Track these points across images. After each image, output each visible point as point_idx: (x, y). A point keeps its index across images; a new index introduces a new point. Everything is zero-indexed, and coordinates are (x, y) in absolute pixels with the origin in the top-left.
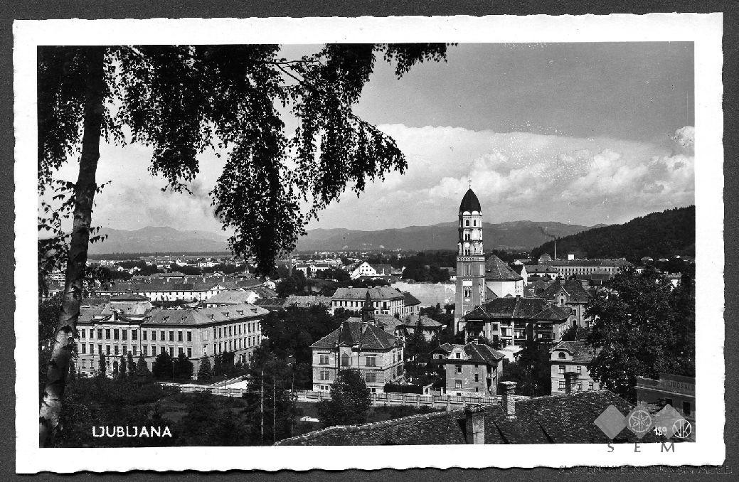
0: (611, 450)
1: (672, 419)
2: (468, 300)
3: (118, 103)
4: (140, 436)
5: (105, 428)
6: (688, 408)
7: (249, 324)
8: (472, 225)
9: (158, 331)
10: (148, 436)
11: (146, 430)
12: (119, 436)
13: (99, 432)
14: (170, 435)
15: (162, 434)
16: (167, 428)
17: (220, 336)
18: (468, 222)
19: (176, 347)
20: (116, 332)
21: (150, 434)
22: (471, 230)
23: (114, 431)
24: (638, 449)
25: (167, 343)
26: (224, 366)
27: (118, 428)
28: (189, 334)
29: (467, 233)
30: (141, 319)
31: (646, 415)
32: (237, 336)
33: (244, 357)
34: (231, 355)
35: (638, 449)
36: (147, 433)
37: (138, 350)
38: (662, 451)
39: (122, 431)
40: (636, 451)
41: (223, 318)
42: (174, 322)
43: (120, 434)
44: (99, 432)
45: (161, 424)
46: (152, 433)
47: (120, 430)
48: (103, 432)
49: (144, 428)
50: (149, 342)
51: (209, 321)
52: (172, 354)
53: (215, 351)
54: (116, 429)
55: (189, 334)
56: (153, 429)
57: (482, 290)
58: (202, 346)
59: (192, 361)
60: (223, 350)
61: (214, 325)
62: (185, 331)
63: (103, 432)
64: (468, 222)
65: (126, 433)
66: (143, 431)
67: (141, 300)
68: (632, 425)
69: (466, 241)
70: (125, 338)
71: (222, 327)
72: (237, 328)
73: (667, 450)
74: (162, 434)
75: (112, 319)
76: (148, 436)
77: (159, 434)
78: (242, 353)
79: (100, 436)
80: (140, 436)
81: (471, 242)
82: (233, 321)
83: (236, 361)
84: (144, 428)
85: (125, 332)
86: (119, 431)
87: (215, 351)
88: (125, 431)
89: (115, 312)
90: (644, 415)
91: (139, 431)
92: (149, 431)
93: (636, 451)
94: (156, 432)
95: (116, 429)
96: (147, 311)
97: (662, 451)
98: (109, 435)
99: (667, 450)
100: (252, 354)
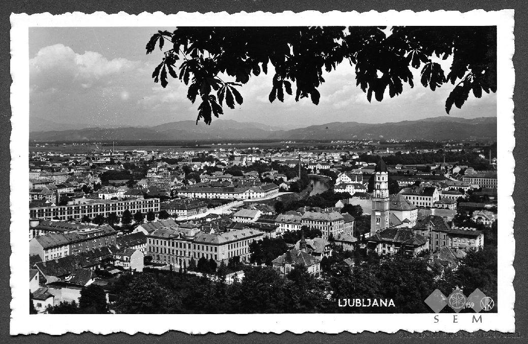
0: (436, 321)
1: (479, 298)
2: (378, 224)
3: (108, 169)
4: (373, 306)
5: (347, 300)
6: (492, 292)
7: (238, 243)
8: (381, 180)
9: (201, 246)
10: (378, 306)
11: (376, 302)
12: (357, 306)
13: (343, 303)
14: (394, 306)
15: (388, 305)
16: (392, 301)
17: (232, 248)
18: (379, 178)
19: (207, 253)
20: (181, 244)
21: (379, 305)
22: (381, 183)
23: (354, 301)
24: (456, 321)
25: (205, 251)
26: (234, 264)
27: (357, 300)
28: (216, 248)
29: (379, 184)
30: (192, 238)
31: (461, 296)
32: (242, 248)
33: (245, 258)
34: (239, 257)
35: (456, 321)
36: (377, 304)
37: (191, 254)
38: (473, 322)
39: (359, 303)
40: (454, 322)
41: (234, 239)
42: (208, 241)
43: (358, 304)
44: (343, 303)
45: (387, 296)
46: (381, 304)
47: (358, 301)
48: (346, 302)
49: (375, 300)
50: (209, 252)
51: (226, 241)
52: (207, 257)
53: (229, 256)
54: (355, 300)
55: (216, 248)
56: (381, 301)
57: (387, 218)
58: (223, 254)
59: (217, 262)
60: (233, 256)
61: (228, 243)
62: (214, 247)
63: (346, 302)
64: (379, 178)
65: (362, 304)
66: (374, 302)
67: (193, 228)
68: (451, 303)
69: (378, 189)
70: (185, 247)
71: (233, 243)
72: (242, 243)
73: (477, 321)
74: (388, 305)
75: (179, 238)
76: (378, 306)
77: (386, 305)
78: (244, 256)
79: (344, 306)
80: (373, 306)
81: (380, 190)
82: (238, 240)
83: (241, 260)
84: (375, 300)
85: (185, 244)
86: (358, 302)
87: (229, 256)
88: (362, 302)
89: (180, 234)
90: (460, 296)
91: (372, 303)
92: (379, 302)
93: (454, 322)
94: (383, 302)
95: (355, 300)
96: (196, 234)
97: (473, 322)
98: (350, 305)
99: (477, 321)
100: (250, 257)
